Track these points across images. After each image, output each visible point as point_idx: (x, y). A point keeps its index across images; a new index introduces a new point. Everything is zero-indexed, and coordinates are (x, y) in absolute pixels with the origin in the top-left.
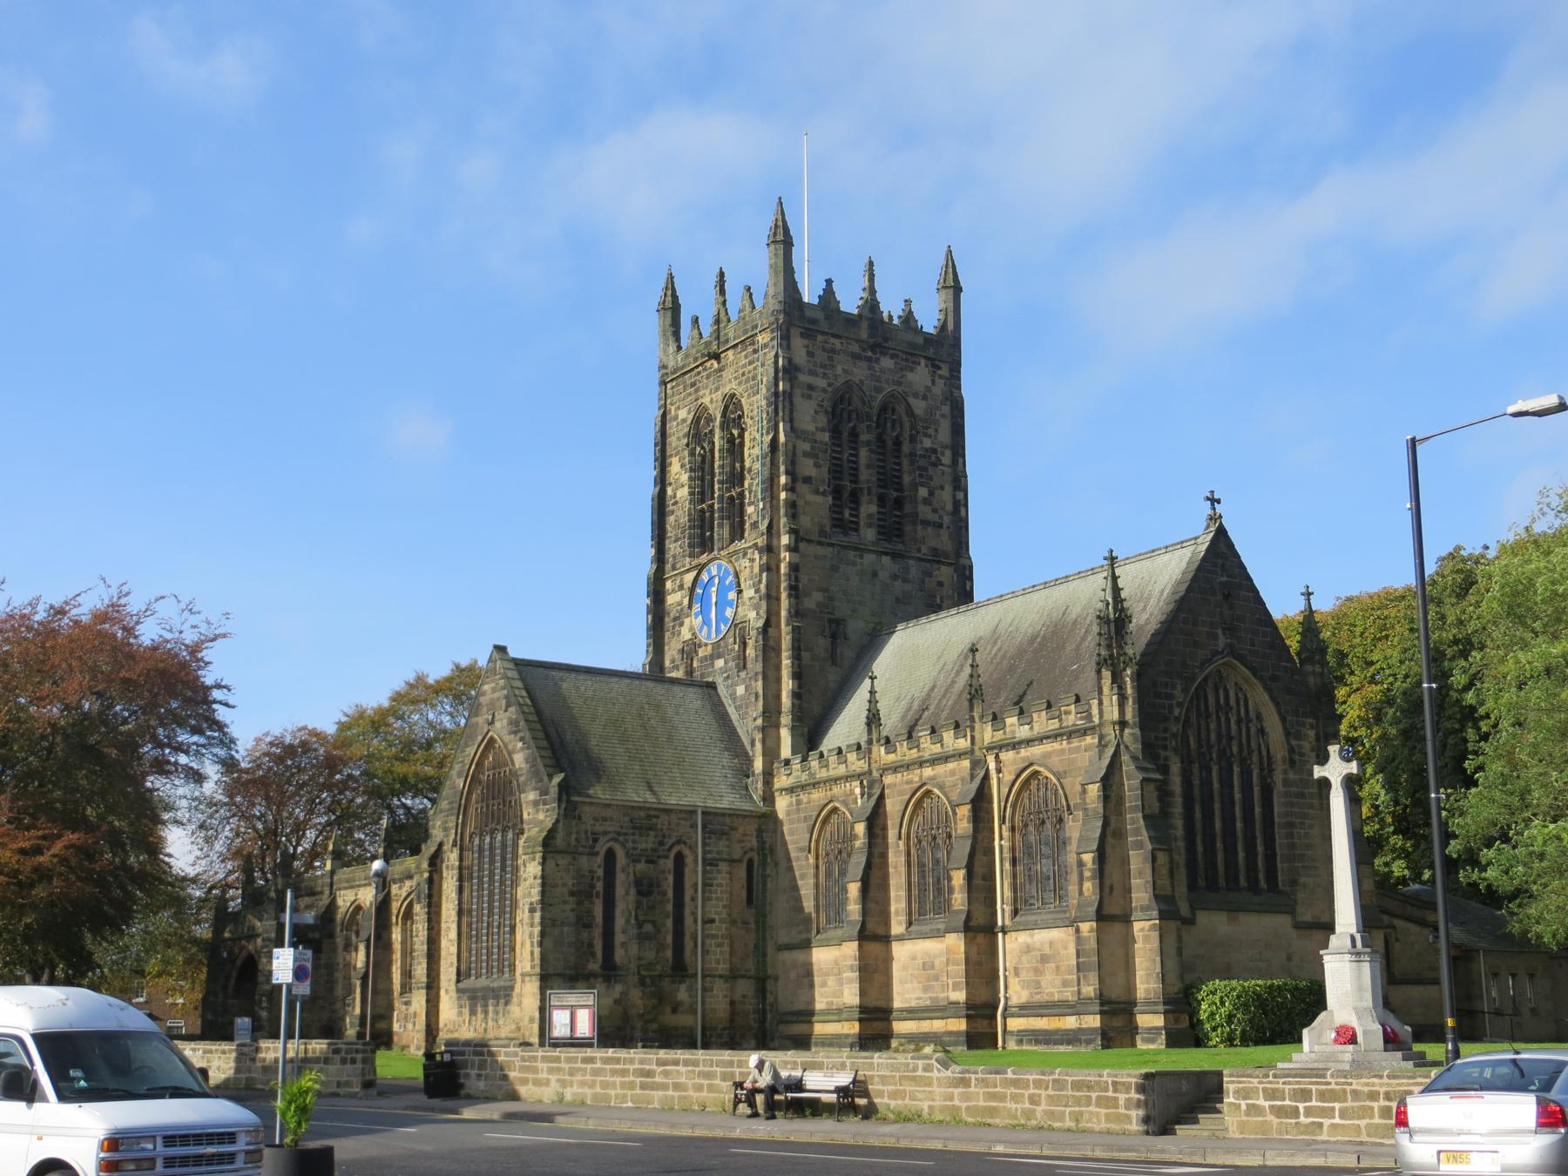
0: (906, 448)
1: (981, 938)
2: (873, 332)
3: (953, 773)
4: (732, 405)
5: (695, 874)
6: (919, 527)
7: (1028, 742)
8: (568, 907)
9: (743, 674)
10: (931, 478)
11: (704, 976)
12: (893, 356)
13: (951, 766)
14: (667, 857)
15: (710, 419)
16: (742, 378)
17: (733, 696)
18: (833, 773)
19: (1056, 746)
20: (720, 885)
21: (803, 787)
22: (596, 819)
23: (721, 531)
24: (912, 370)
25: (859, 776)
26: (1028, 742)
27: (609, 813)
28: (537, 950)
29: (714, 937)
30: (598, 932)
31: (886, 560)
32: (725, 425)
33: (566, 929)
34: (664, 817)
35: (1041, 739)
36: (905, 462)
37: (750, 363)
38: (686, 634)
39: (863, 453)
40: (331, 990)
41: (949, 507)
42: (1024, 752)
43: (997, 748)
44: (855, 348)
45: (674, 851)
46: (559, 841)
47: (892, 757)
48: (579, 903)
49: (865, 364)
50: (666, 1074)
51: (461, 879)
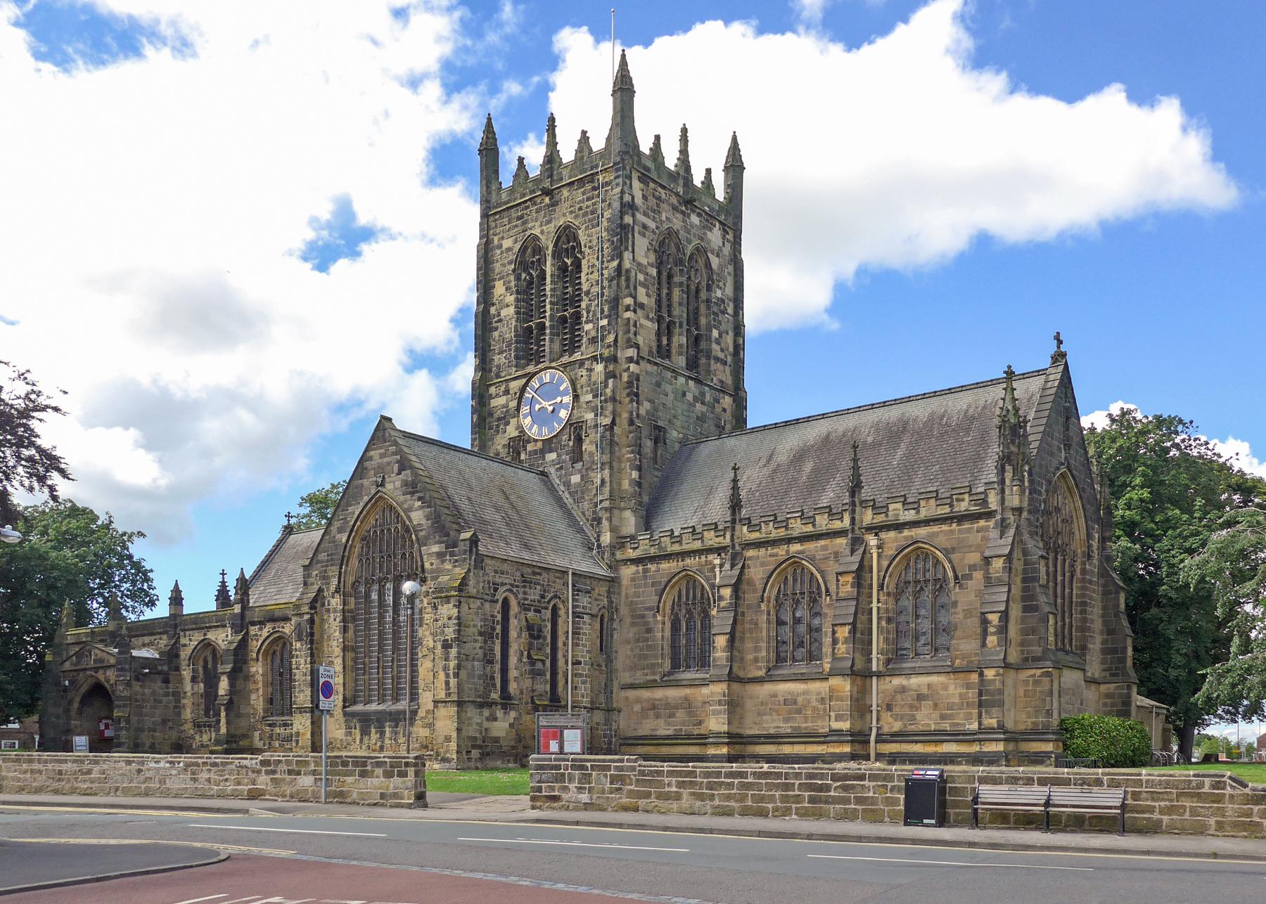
0: (703, 295)
2: (679, 188)
3: (824, 548)
5: (566, 624)
6: (712, 362)
9: (579, 465)
10: (720, 323)
11: (573, 707)
12: (699, 215)
13: (822, 542)
14: (546, 608)
15: (538, 250)
16: (578, 212)
17: (567, 484)
18: (686, 547)
19: (945, 527)
20: (585, 634)
21: (653, 559)
23: (549, 344)
24: (711, 230)
25: (719, 550)
27: (505, 567)
28: (453, 682)
29: (581, 675)
30: (498, 667)
31: (691, 383)
32: (557, 254)
34: (545, 575)
35: (927, 522)
36: (703, 308)
37: (588, 199)
38: (511, 431)
40: (179, 714)
41: (731, 349)
42: (906, 533)
43: (876, 529)
44: (674, 200)
46: (472, 589)
48: (485, 642)
49: (680, 216)
50: (846, 788)
51: (344, 620)
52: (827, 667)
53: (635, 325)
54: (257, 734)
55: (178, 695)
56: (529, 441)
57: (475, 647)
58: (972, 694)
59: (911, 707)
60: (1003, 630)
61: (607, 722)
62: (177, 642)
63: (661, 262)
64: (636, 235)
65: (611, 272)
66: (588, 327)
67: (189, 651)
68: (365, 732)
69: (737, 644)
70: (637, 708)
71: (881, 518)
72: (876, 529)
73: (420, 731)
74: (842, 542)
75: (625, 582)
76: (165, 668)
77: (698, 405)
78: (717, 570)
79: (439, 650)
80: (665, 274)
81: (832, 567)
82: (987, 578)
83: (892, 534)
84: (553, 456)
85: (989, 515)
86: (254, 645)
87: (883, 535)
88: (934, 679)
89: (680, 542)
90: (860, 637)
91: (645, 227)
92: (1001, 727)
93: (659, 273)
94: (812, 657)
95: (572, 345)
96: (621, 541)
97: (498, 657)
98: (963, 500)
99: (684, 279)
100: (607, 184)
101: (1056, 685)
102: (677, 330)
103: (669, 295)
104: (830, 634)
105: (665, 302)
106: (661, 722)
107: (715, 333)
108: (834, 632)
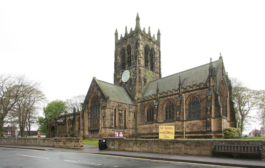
0: (153, 56)
2: (148, 37)
3: (174, 97)
8: (109, 117)
9: (131, 86)
12: (152, 42)
13: (174, 96)
14: (123, 111)
15: (124, 50)
17: (129, 90)
19: (198, 91)
22: (113, 104)
23: (127, 66)
25: (155, 99)
32: (127, 50)
33: (109, 120)
34: (123, 104)
35: (194, 90)
36: (153, 59)
37: (132, 39)
39: (148, 55)
40: (66, 131)
42: (190, 93)
44: (148, 39)
45: (125, 109)
47: (161, 96)
52: (175, 120)
53: (140, 60)
54: (77, 134)
55: (66, 128)
56: (123, 83)
58: (204, 124)
59: (192, 127)
61: (136, 131)
62: (66, 119)
63: (145, 50)
64: (140, 45)
65: (135, 51)
66: (132, 62)
67: (67, 120)
68: (91, 134)
69: (158, 116)
70: (141, 129)
71: (185, 90)
72: (184, 93)
73: (100, 133)
74: (178, 95)
75: (139, 106)
76: (64, 123)
77: (153, 75)
78: (155, 103)
79: (102, 118)
80: (146, 52)
81: (176, 100)
82: (207, 100)
83: (187, 93)
84: (127, 85)
85: (207, 88)
86: (76, 119)
87: (186, 94)
88: (196, 121)
89: (148, 98)
91: (142, 43)
93: (145, 52)
94: (173, 118)
95: (130, 65)
97: (114, 119)
98: (202, 85)
99: (150, 53)
100: (135, 36)
102: (149, 62)
103: (147, 56)
104: (175, 113)
105: (146, 57)
106: (145, 131)
107: (156, 63)
108: (176, 113)
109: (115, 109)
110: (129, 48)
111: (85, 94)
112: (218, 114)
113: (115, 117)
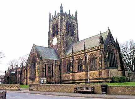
1: (86, 72)
2: (69, 16)
4: (57, 23)
5: (54, 67)
7: (91, 51)
23: (55, 34)
25: (71, 56)
26: (91, 51)
32: (56, 25)
35: (93, 51)
39: (69, 28)
42: (91, 53)
46: (41, 63)
47: (75, 54)
57: (41, 70)
60: (101, 64)
71: (88, 51)
74: (84, 54)
75: (62, 61)
90: (86, 66)
92: (102, 78)
96: (62, 56)
101: (109, 71)
109: (46, 64)
110: (57, 24)
111: (29, 53)
112: (106, 67)
113: (46, 70)
